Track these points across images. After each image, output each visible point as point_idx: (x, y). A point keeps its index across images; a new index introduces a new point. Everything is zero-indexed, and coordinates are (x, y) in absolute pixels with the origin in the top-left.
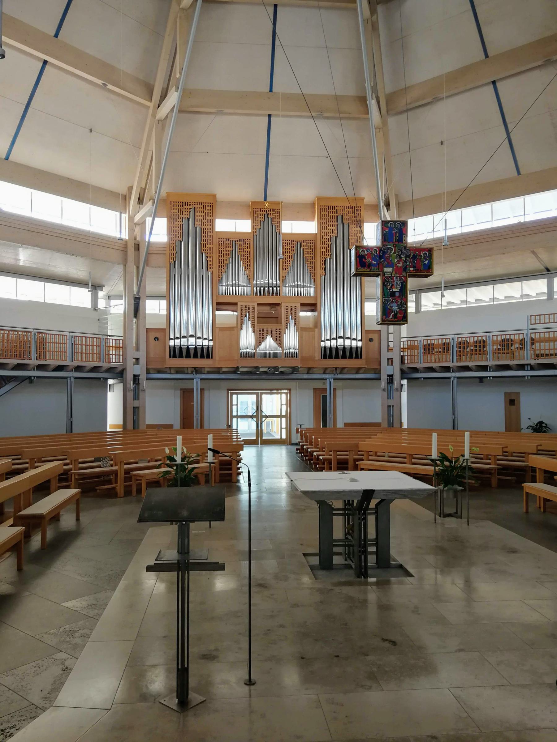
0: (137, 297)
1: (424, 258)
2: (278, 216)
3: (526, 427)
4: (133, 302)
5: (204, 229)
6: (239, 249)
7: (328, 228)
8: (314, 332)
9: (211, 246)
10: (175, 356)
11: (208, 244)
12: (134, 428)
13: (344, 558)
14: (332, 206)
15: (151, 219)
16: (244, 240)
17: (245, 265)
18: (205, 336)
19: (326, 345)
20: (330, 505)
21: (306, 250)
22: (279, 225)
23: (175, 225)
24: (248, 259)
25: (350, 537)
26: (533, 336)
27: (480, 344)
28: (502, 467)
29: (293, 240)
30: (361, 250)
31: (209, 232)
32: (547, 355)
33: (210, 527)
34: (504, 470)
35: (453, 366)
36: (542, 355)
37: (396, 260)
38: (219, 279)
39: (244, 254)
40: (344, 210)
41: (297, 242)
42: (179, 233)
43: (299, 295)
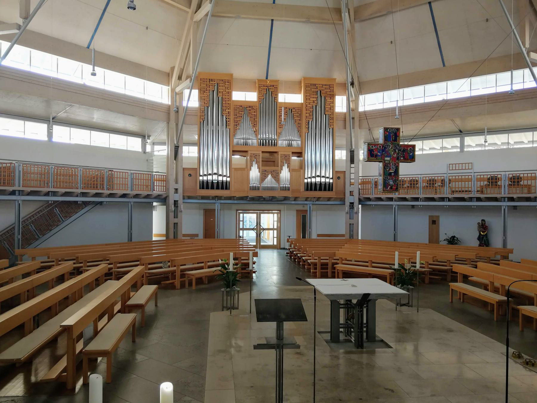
0: (177, 145)
1: (410, 151)
2: (276, 90)
3: (444, 240)
4: (174, 149)
5: (225, 98)
7: (311, 99)
8: (300, 173)
9: (229, 111)
10: (203, 188)
12: (174, 238)
13: (345, 335)
14: (314, 84)
15: (189, 90)
16: (252, 106)
17: (253, 124)
18: (225, 174)
19: (308, 181)
20: (338, 301)
23: (204, 96)
24: (254, 120)
25: (349, 322)
28: (432, 270)
30: (371, 146)
31: (228, 101)
33: (250, 313)
34: (434, 272)
35: (396, 197)
36: (456, 191)
37: (393, 153)
38: (234, 134)
39: (252, 117)
40: (322, 87)
41: (289, 109)
43: (290, 146)
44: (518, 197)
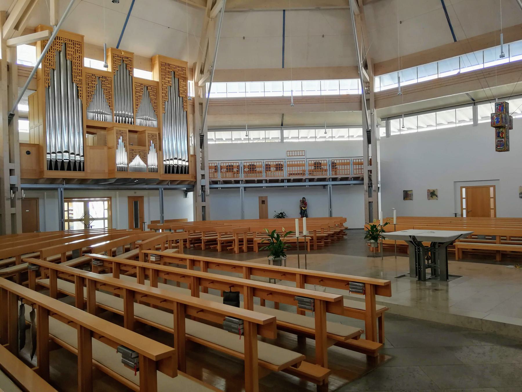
5: (75, 63)
6: (102, 84)
9: (81, 78)
11: (78, 76)
16: (106, 77)
21: (151, 93)
22: (131, 70)
24: (109, 93)
26: (222, 165)
27: (318, 165)
29: (142, 84)
31: (79, 66)
32: (296, 174)
39: (106, 89)
42: (53, 62)
44: (234, 181)
